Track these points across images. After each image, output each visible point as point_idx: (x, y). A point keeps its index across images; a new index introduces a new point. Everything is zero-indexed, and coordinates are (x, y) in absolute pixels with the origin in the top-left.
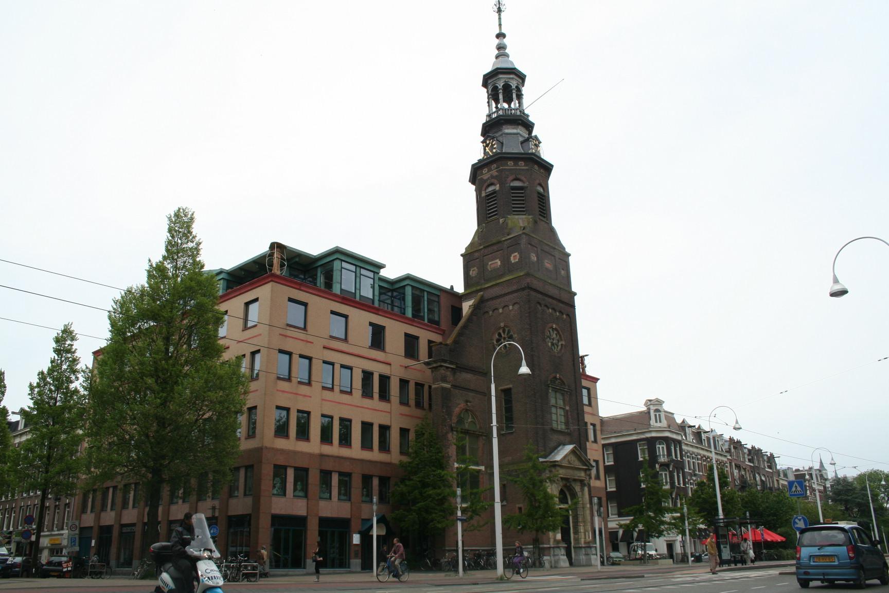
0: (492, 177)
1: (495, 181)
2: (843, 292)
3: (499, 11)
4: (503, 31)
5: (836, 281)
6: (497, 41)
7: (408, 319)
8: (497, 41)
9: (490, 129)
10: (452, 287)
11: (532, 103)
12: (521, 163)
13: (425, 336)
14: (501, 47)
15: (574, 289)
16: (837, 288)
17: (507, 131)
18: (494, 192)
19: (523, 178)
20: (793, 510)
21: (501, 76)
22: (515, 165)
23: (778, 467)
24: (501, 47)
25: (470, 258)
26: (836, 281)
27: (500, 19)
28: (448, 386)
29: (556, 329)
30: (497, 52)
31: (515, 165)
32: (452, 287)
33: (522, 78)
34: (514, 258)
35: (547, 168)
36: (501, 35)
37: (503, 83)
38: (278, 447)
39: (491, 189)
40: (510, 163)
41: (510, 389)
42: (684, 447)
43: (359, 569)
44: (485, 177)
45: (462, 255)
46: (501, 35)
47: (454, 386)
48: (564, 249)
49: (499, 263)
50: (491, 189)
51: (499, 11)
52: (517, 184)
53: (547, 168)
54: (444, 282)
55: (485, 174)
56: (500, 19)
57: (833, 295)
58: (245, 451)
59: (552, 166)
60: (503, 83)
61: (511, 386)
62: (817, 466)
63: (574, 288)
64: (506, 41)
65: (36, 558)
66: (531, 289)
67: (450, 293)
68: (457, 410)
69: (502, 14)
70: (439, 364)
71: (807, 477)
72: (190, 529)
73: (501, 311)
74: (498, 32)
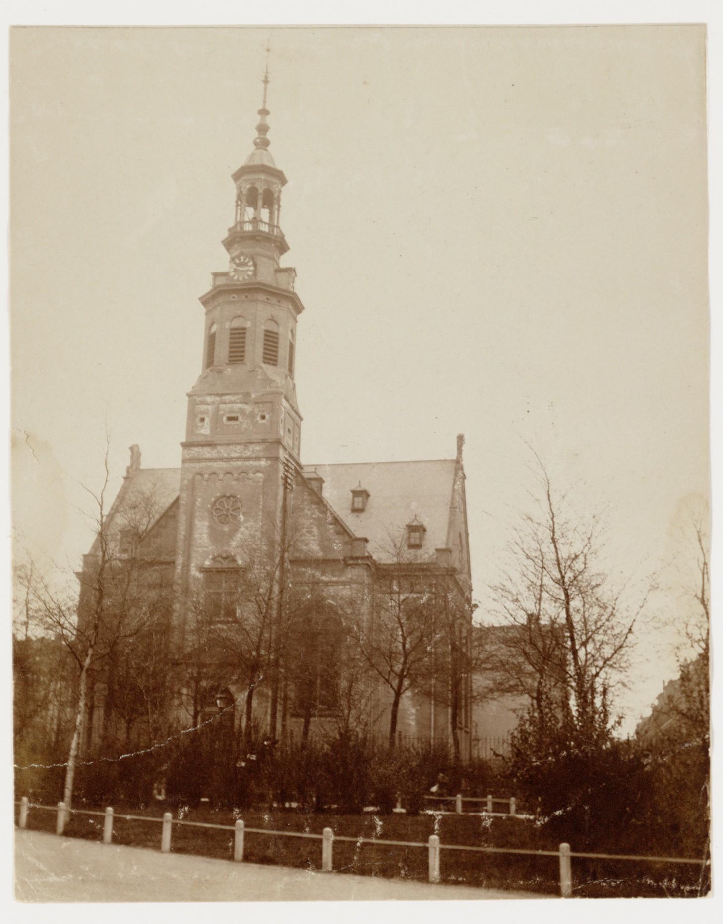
4: (268, 108)
6: (258, 119)
8: (258, 119)
9: (235, 240)
11: (291, 219)
14: (263, 129)
20: (320, 602)
24: (263, 129)
30: (222, 261)
33: (281, 179)
36: (264, 112)
37: (260, 186)
43: (21, 637)
46: (264, 112)
51: (266, 81)
58: (211, 431)
59: (304, 308)
60: (260, 186)
64: (269, 120)
65: (471, 635)
69: (269, 85)
72: (566, 660)
74: (261, 107)
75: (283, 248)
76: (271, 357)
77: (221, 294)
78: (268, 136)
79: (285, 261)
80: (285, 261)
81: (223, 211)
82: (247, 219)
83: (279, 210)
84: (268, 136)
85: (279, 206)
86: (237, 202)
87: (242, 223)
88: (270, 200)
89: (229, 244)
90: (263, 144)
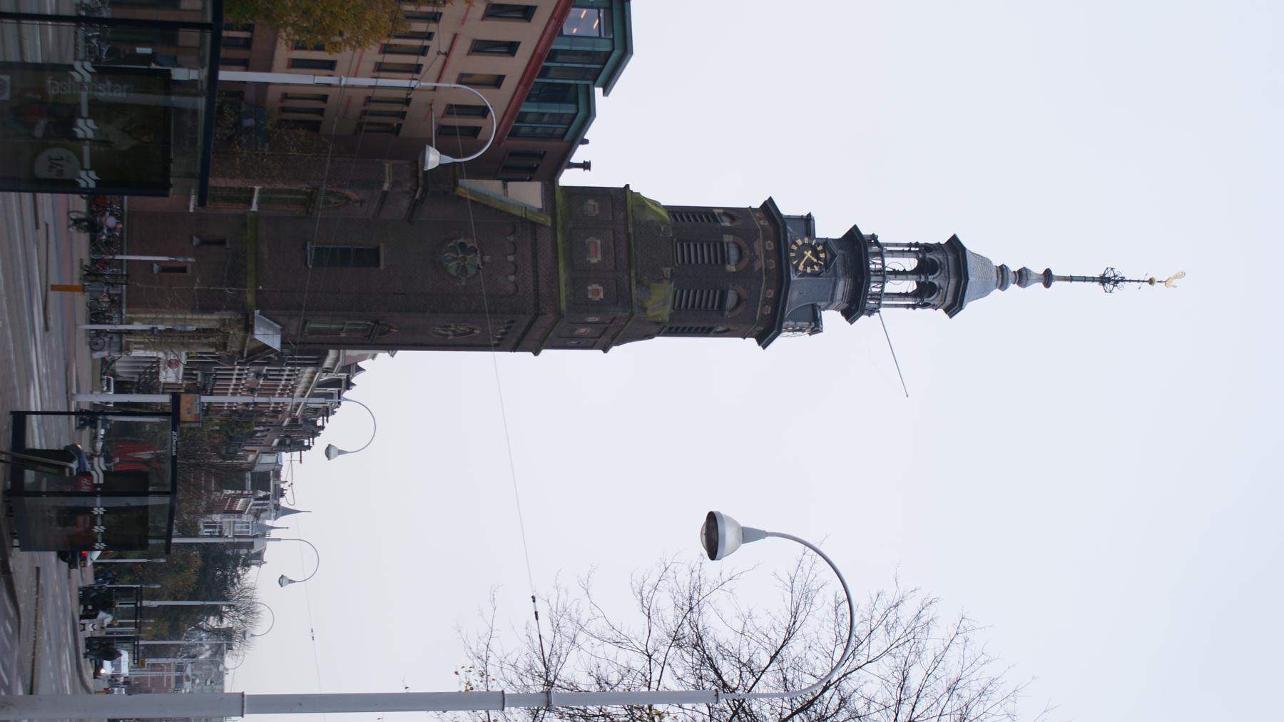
0: (754, 259)
1: (743, 265)
2: (713, 547)
3: (1103, 280)
4: (1055, 284)
5: (749, 535)
7: (519, 104)
10: (586, 142)
11: (902, 328)
12: (768, 310)
13: (496, 101)
14: (1022, 277)
15: (545, 352)
16: (729, 535)
17: (841, 284)
18: (725, 260)
19: (739, 310)
21: (953, 282)
22: (766, 299)
23: (285, 456)
24: (1022, 277)
25: (619, 198)
26: (749, 535)
27: (1085, 279)
28: (386, 187)
29: (472, 332)
31: (766, 299)
32: (586, 142)
33: (953, 308)
34: (596, 291)
35: (764, 339)
36: (1048, 278)
37: (946, 275)
38: (279, 45)
39: (733, 254)
40: (771, 293)
41: (377, 264)
42: (310, 369)
44: (758, 246)
45: (627, 186)
46: (1048, 278)
47: (385, 194)
48: (618, 344)
49: (594, 261)
50: (733, 254)
51: (1103, 280)
52: (731, 299)
53: (764, 339)
54: (612, 110)
55: (763, 246)
56: (1085, 279)
57: (712, 520)
60: (946, 275)
61: (382, 266)
62: (283, 502)
63: (545, 353)
66: (537, 315)
67: (563, 162)
68: (348, 192)
69: (1121, 271)
70: (421, 182)
71: (262, 494)
73: (511, 258)
74: (1041, 285)
75: (851, 314)
76: (324, 98)
77: (7, 493)
78: (1013, 288)
79: (831, 318)
80: (831, 318)
81: (901, 222)
82: (888, 261)
83: (908, 306)
84: (1013, 288)
85: (914, 307)
86: (917, 245)
87: (881, 254)
88: (923, 296)
89: (854, 234)
90: (1003, 277)
